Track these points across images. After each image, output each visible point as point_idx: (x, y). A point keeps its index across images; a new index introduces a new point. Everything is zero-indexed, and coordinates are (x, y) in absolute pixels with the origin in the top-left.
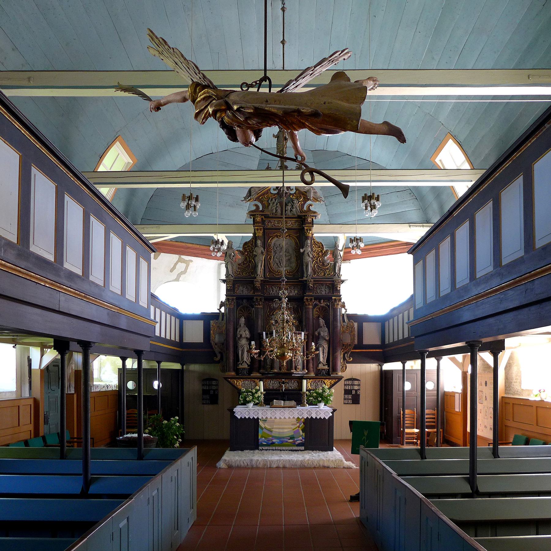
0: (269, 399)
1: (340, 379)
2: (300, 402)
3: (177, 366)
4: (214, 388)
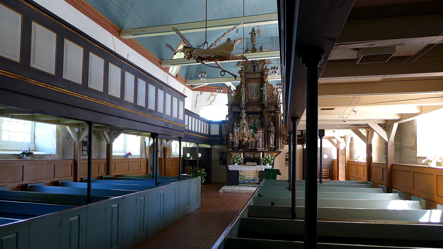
0: (246, 161)
1: (280, 152)
2: (259, 164)
3: (208, 146)
4: (225, 157)
